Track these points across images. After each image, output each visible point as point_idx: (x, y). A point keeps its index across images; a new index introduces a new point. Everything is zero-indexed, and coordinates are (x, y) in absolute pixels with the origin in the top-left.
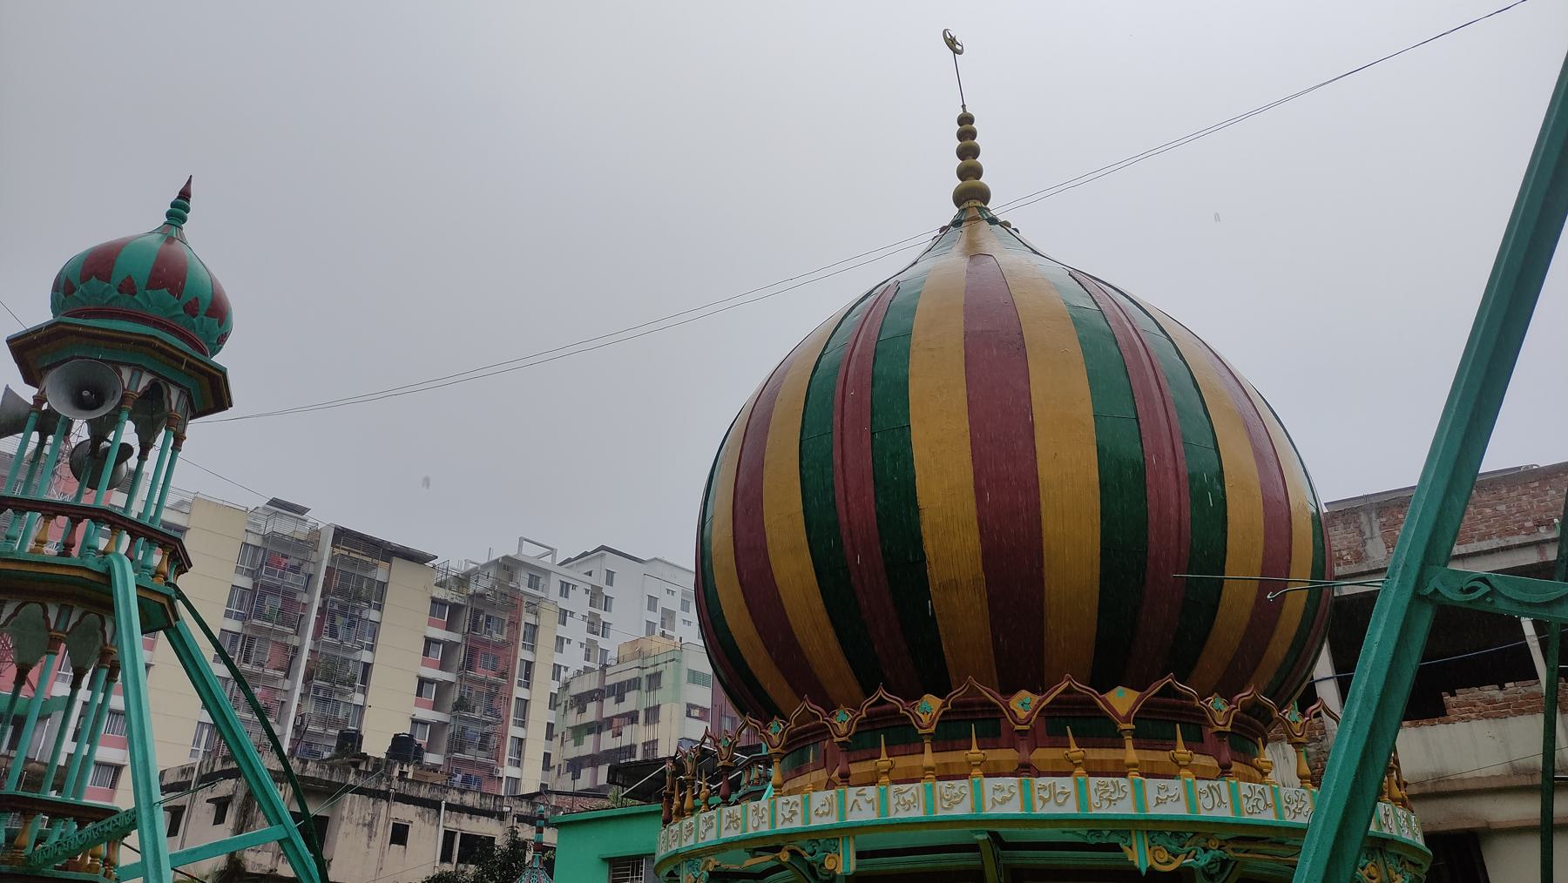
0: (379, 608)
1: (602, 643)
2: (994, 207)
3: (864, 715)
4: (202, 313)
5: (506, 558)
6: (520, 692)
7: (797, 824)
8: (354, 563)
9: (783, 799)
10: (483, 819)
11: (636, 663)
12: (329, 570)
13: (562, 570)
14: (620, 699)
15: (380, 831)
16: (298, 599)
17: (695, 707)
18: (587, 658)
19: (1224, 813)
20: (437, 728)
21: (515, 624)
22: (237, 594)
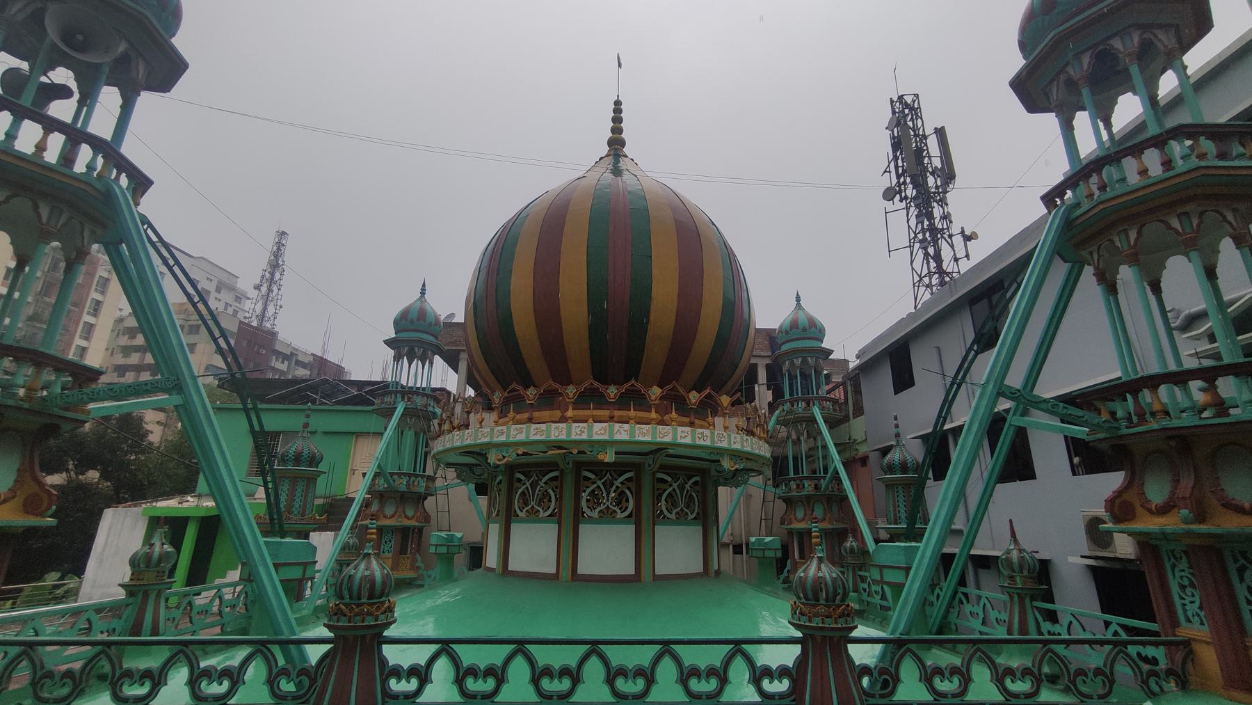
3: (624, 391)
6: (87, 318)
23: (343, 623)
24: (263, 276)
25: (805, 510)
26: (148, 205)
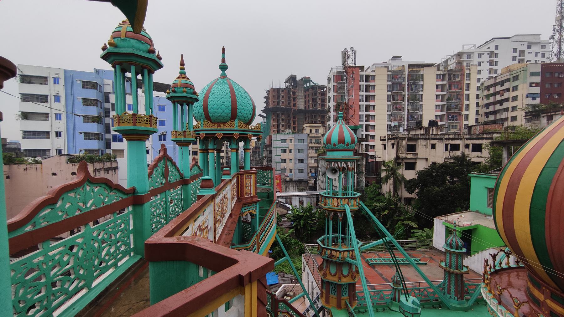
1: (495, 68)
5: (459, 53)
8: (414, 71)
10: (455, 140)
11: (508, 74)
12: (408, 75)
15: (428, 146)
16: (402, 84)
18: (490, 73)
20: (442, 116)
21: (462, 75)
22: (389, 86)
24: (554, 30)
26: (8, 141)
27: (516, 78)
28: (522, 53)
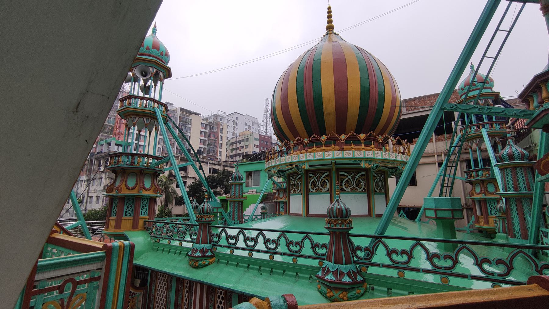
0: (191, 125)
2: (335, 30)
4: (164, 55)
5: (215, 114)
6: (220, 142)
7: (297, 160)
9: (294, 156)
10: (217, 166)
11: (244, 136)
13: (227, 117)
14: (240, 144)
17: (256, 145)
18: (233, 135)
19: (380, 157)
21: (218, 128)
23: (332, 226)
24: (264, 117)
25: (481, 188)
27: (247, 140)
28: (249, 126)
